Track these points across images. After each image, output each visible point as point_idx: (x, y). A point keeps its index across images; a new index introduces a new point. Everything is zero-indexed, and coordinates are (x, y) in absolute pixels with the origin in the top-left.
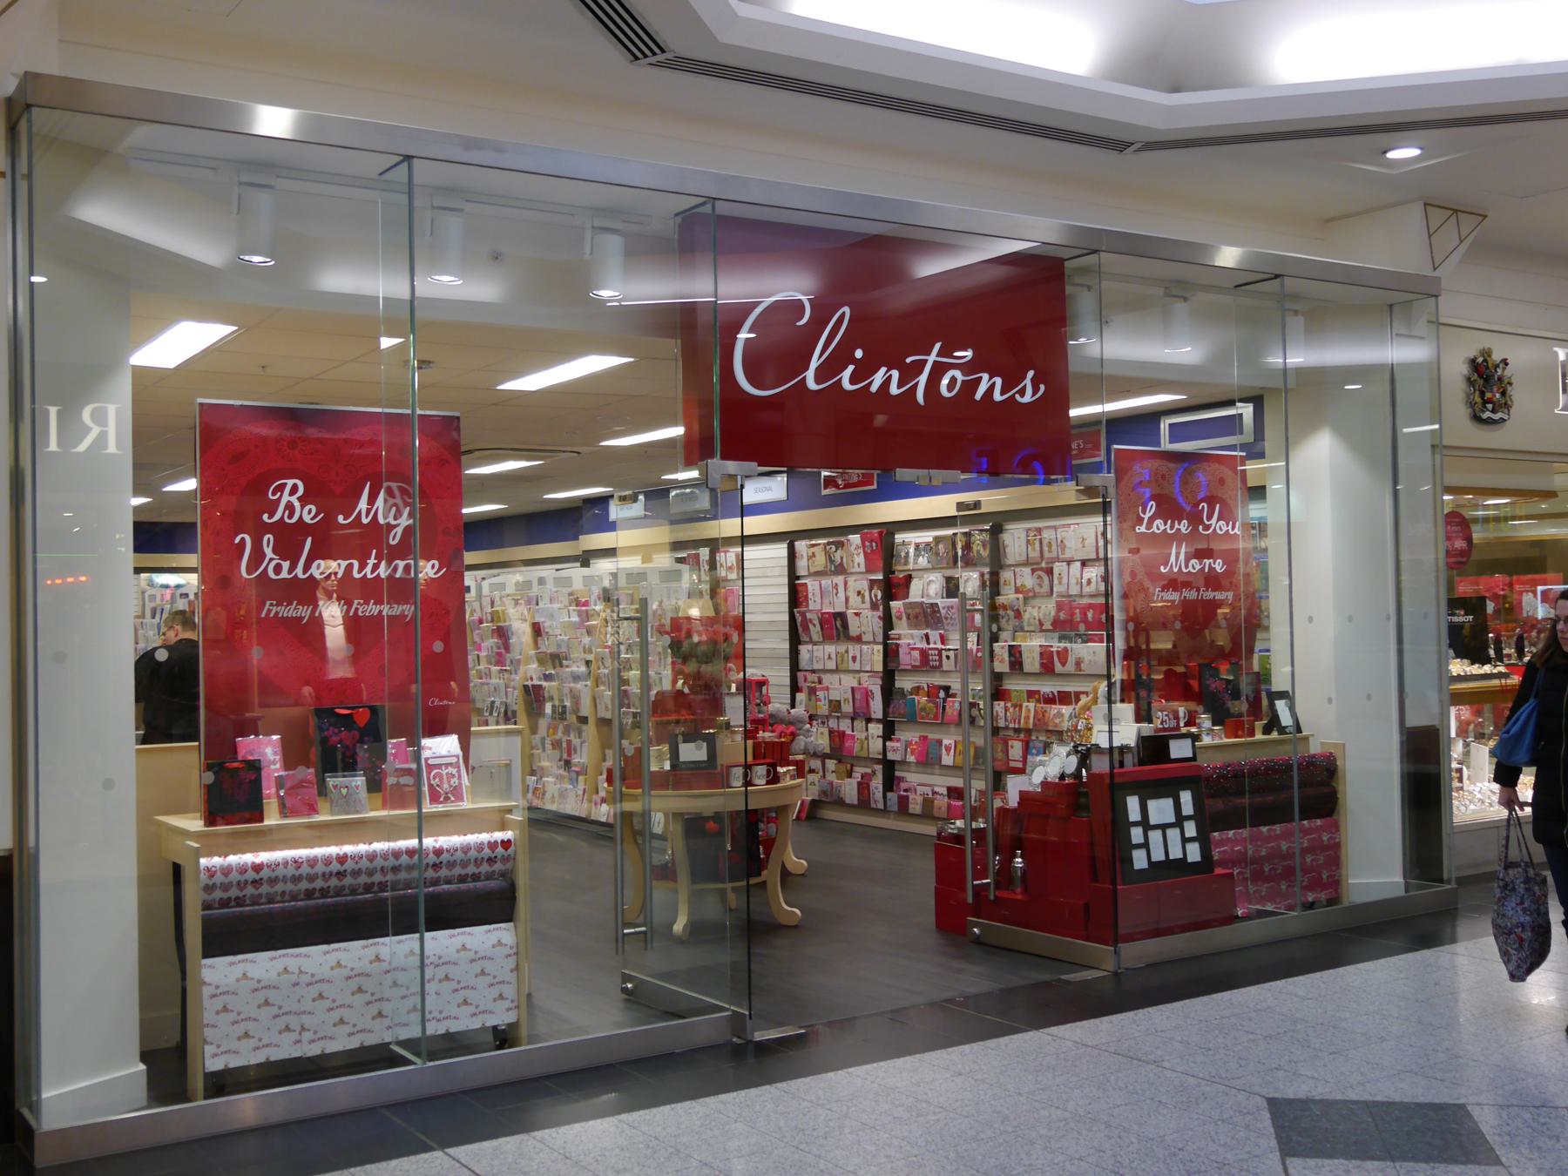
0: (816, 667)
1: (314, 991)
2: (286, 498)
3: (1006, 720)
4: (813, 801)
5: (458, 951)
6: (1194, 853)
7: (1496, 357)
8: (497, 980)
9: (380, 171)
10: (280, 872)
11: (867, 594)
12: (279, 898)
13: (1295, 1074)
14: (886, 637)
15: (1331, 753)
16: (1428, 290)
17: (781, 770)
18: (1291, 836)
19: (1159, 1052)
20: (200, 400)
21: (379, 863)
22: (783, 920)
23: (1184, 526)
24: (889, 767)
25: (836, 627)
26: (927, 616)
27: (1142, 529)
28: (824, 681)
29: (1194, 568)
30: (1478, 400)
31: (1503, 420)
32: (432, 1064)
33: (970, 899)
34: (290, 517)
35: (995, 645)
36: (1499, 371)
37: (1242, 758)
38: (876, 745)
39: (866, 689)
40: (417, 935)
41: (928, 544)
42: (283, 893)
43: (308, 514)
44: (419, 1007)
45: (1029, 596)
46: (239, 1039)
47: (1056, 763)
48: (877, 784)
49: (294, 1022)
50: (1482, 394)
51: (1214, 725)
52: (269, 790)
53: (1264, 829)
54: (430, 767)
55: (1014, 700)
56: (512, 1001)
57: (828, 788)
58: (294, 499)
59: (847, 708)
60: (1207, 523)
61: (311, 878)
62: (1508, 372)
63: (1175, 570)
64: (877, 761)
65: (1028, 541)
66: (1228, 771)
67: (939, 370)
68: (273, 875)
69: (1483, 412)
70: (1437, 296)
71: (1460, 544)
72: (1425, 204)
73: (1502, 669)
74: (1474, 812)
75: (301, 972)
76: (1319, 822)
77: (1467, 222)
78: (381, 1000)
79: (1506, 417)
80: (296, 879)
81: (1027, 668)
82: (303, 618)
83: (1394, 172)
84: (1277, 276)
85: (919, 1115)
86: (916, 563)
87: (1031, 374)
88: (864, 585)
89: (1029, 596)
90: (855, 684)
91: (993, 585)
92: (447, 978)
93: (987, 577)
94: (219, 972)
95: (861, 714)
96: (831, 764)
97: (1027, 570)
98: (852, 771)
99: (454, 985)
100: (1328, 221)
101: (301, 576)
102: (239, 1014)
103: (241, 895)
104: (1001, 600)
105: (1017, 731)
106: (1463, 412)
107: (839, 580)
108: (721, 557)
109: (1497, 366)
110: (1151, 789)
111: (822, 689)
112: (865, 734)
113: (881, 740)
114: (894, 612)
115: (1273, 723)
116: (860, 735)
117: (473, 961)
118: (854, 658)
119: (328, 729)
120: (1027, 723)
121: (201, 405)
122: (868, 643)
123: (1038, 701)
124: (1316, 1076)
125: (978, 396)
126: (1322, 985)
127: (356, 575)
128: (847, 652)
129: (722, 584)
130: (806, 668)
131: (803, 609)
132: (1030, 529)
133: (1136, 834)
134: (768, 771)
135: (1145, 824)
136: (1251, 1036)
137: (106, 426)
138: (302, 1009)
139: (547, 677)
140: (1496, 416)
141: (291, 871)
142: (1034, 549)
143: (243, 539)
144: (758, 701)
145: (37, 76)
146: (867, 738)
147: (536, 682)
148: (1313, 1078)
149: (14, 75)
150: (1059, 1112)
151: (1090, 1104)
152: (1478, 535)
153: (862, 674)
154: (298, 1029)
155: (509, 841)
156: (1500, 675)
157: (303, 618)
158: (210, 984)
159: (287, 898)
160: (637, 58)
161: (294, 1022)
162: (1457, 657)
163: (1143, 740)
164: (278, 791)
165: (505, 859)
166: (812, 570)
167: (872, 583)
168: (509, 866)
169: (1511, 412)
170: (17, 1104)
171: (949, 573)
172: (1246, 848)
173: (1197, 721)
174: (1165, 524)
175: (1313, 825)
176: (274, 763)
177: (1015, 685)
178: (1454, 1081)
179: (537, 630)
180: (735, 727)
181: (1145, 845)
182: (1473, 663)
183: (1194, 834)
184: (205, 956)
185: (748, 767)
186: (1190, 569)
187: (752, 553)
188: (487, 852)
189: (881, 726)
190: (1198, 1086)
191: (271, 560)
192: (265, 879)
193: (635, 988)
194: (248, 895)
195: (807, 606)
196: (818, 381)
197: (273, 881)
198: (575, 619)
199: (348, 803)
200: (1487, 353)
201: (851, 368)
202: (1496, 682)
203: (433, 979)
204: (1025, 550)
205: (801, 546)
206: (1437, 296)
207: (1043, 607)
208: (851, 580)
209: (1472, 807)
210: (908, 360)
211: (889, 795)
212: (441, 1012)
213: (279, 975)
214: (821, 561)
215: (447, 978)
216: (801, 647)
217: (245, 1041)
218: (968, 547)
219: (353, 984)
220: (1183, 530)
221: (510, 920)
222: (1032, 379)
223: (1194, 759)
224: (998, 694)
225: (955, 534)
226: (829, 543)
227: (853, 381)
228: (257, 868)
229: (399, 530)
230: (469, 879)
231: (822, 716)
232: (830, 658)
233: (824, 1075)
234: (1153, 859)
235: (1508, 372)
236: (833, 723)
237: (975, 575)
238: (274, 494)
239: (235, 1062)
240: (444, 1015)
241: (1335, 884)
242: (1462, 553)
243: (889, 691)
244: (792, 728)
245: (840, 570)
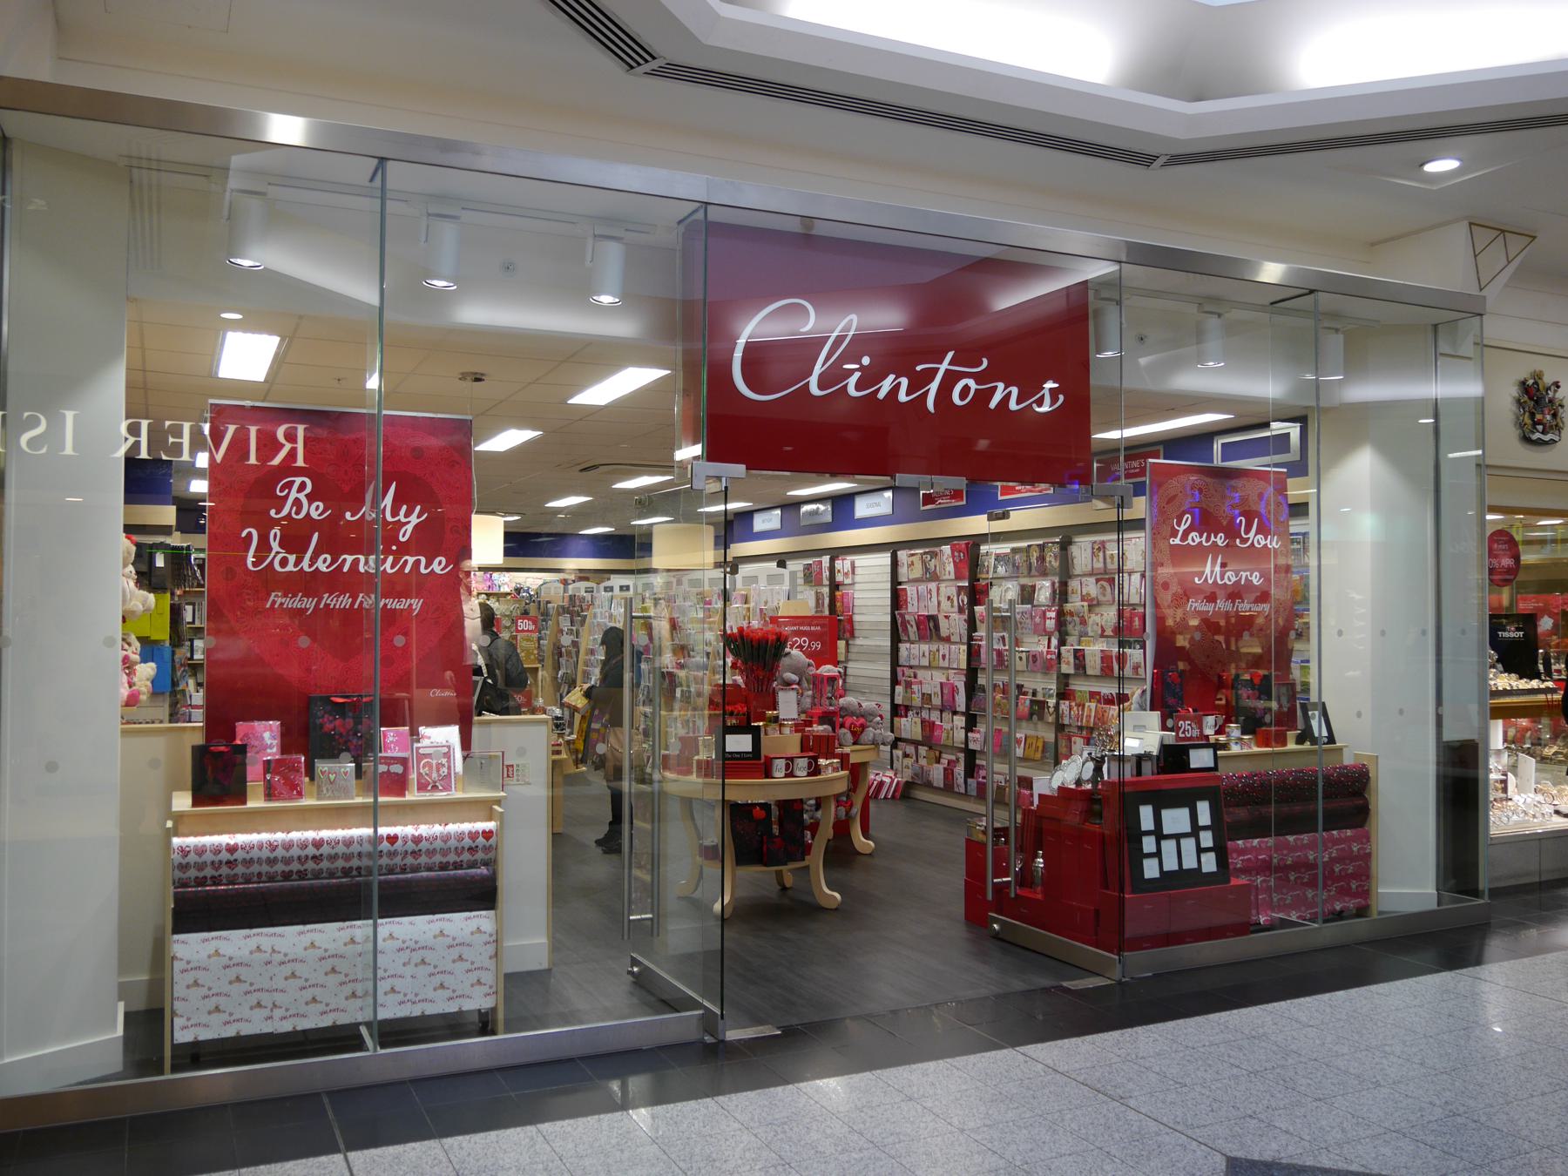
0: (914, 662)
1: (287, 970)
2: (293, 494)
3: (1070, 718)
4: (907, 782)
5: (435, 937)
6: (1209, 863)
7: (1548, 379)
8: (437, 970)
9: (369, 177)
10: (255, 854)
11: (955, 599)
12: (255, 879)
13: (1269, 1125)
14: (970, 638)
15: (1364, 765)
16: (1473, 310)
17: (822, 762)
18: (1316, 846)
19: (1131, 1085)
20: (212, 401)
21: (355, 848)
22: (824, 903)
23: (1220, 540)
24: (971, 755)
25: (929, 627)
26: (1002, 622)
27: (1177, 541)
28: (918, 676)
29: (1230, 580)
30: (1528, 421)
31: (1554, 442)
32: (383, 1051)
33: (990, 897)
34: (297, 513)
35: (1063, 648)
36: (1551, 394)
37: (1271, 768)
38: (960, 735)
39: (952, 684)
40: (371, 922)
41: (1006, 555)
42: (260, 874)
43: (316, 511)
44: (371, 992)
45: (1093, 605)
46: (210, 1013)
47: (1072, 771)
48: (960, 770)
49: (266, 999)
50: (1532, 415)
51: (1243, 733)
52: (254, 770)
53: (1291, 838)
54: (421, 757)
55: (1078, 701)
56: (491, 987)
57: (920, 771)
58: (302, 496)
59: (937, 701)
60: (1245, 536)
61: (287, 861)
62: (1559, 395)
63: (1210, 582)
64: (961, 750)
65: (1093, 553)
66: (1254, 781)
67: (950, 379)
68: (248, 857)
69: (1533, 433)
70: (1481, 315)
71: (1507, 562)
72: (1471, 224)
73: (1550, 684)
74: (1516, 823)
75: (274, 951)
76: (1349, 833)
77: (1515, 243)
78: (355, 981)
79: (1557, 438)
80: (272, 861)
81: (1089, 672)
82: (307, 610)
83: (1435, 188)
84: (1312, 292)
85: (844, 1151)
86: (995, 572)
88: (953, 591)
89: (1093, 605)
90: (944, 680)
91: (1061, 594)
92: (423, 962)
93: (1057, 585)
94: (191, 947)
95: (948, 707)
96: (923, 750)
97: (1092, 580)
98: (940, 757)
99: (430, 969)
100: (1373, 244)
101: (306, 569)
102: (251, 984)
103: (216, 874)
104: (1068, 607)
105: (1080, 728)
106: (1513, 433)
107: (933, 586)
108: (838, 564)
109: (1549, 388)
110: (1162, 800)
111: (916, 683)
112: (951, 725)
113: (963, 731)
114: (977, 615)
115: (1306, 736)
116: (947, 726)
117: (450, 947)
118: (944, 657)
119: (323, 716)
120: (1088, 721)
121: (212, 405)
122: (956, 643)
123: (1099, 702)
124: (1291, 1129)
125: (993, 405)
126: (1328, 1010)
127: (423, 571)
128: (938, 650)
129: (840, 588)
130: (905, 664)
131: (903, 611)
132: (1095, 542)
133: (1149, 844)
134: (810, 763)
135: (1159, 834)
136: (1235, 1071)
137: (296, 443)
138: (275, 987)
139: (681, 666)
140: (1547, 438)
141: (266, 853)
142: (1098, 561)
143: (250, 534)
144: (830, 695)
146: (952, 729)
147: (670, 670)
148: (1287, 1132)
150: (995, 1158)
151: (1031, 1150)
152: (1528, 557)
153: (950, 671)
154: (270, 1005)
155: (491, 832)
156: (1547, 691)
157: (307, 610)
158: (182, 960)
159: (264, 878)
160: (632, 67)
161: (266, 999)
162: (1505, 671)
163: (1164, 748)
164: (265, 775)
165: (487, 849)
166: (911, 577)
167: (960, 589)
168: (491, 855)
169: (1562, 435)
171: (1027, 581)
172: (1271, 857)
173: (1227, 730)
174: (1201, 537)
175: (1343, 836)
176: (271, 747)
177: (1080, 686)
178: (1446, 1148)
179: (674, 625)
180: (616, 735)
181: (1158, 854)
182: (1521, 678)
183: (1210, 844)
184: (176, 930)
185: (790, 760)
186: (1226, 580)
187: (862, 560)
188: (467, 842)
189: (964, 718)
190: (1158, 1134)
191: (278, 553)
192: (240, 860)
193: (640, 973)
194: (224, 875)
195: (907, 608)
196: (821, 387)
197: (248, 862)
198: (701, 615)
199: (337, 789)
200: (1538, 376)
202: (1542, 697)
203: (409, 963)
204: (1090, 561)
205: (902, 555)
206: (1481, 315)
207: (1105, 614)
208: (942, 586)
209: (1515, 818)
210: (919, 368)
211: (970, 780)
212: (416, 995)
213: (251, 953)
214: (917, 572)
215: (423, 962)
216: (900, 645)
217: (215, 1016)
218: (1042, 559)
219: (328, 965)
220: (1220, 543)
221: (492, 908)
223: (1215, 768)
224: (1064, 694)
225: (1029, 546)
226: (925, 553)
227: (858, 387)
228: (232, 849)
229: (410, 528)
230: (451, 867)
231: (916, 708)
232: (924, 655)
233: (772, 1089)
234: (1165, 869)
235: (1559, 395)
236: (925, 714)
237: (1047, 584)
238: (281, 491)
239: (205, 1035)
240: (419, 997)
241: (1365, 893)
242: (1509, 571)
243: (972, 687)
244: (862, 720)
245: (934, 577)
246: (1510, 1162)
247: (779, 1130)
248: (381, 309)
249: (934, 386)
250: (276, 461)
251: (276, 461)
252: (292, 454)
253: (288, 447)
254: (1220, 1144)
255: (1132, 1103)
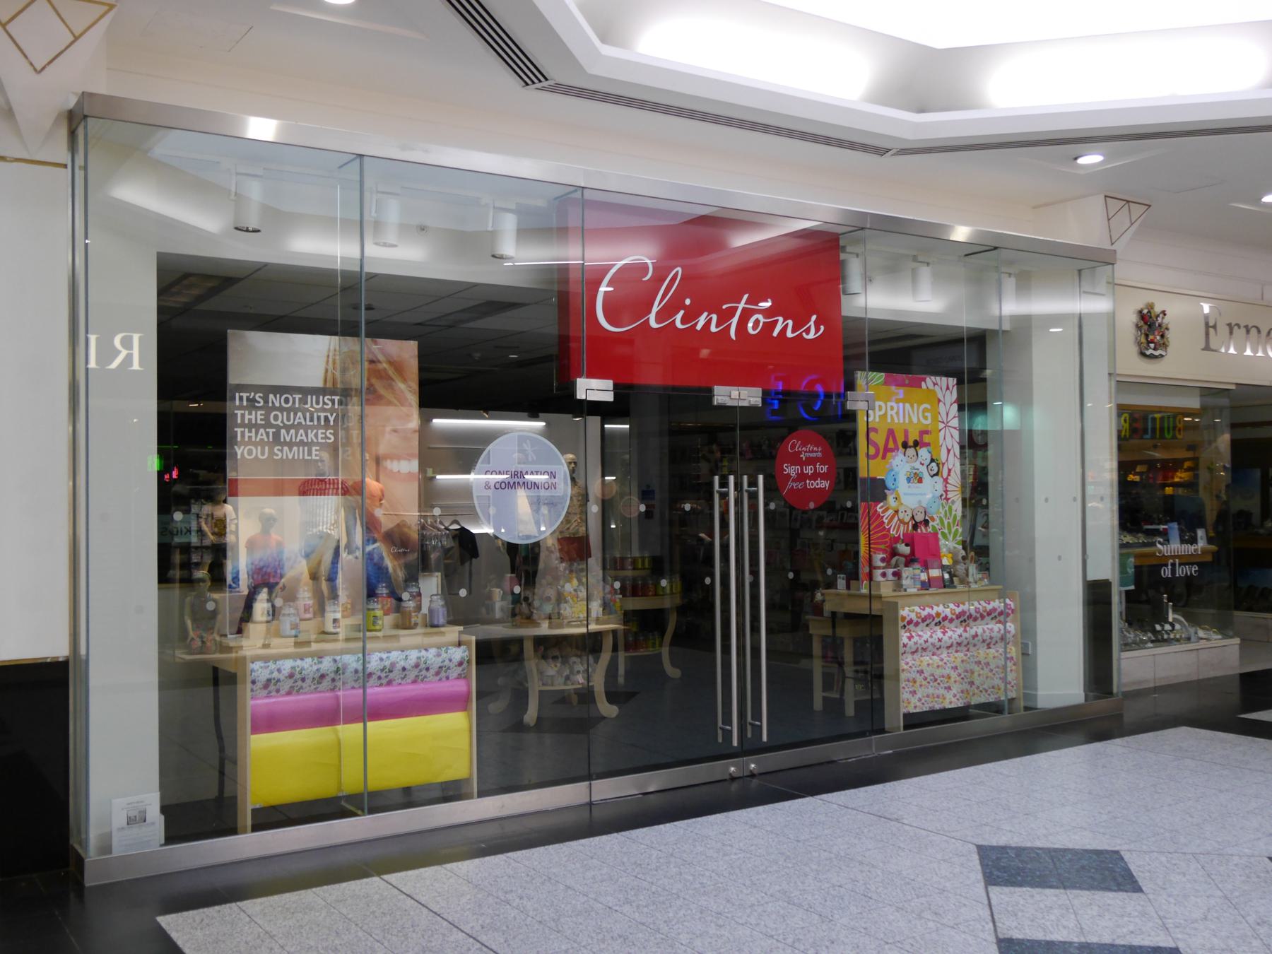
7: (1158, 309)
30: (1143, 340)
31: (1162, 356)
36: (1160, 319)
50: (1147, 336)
67: (746, 315)
69: (1147, 349)
72: (1106, 196)
77: (1137, 210)
79: (1164, 353)
84: (996, 248)
87: (814, 318)
106: (1134, 350)
109: (1158, 316)
124: (1013, 829)
125: (775, 334)
136: (968, 802)
140: (1157, 353)
145: (91, 95)
148: (1010, 831)
149: (75, 94)
170: (71, 842)
200: (1150, 306)
201: (682, 312)
210: (724, 307)
222: (815, 322)
246: (1153, 839)
247: (675, 847)
248: (362, 260)
249: (735, 321)
250: (114, 365)
251: (114, 365)
252: (129, 358)
253: (124, 353)
254: (969, 839)
255: (905, 821)
